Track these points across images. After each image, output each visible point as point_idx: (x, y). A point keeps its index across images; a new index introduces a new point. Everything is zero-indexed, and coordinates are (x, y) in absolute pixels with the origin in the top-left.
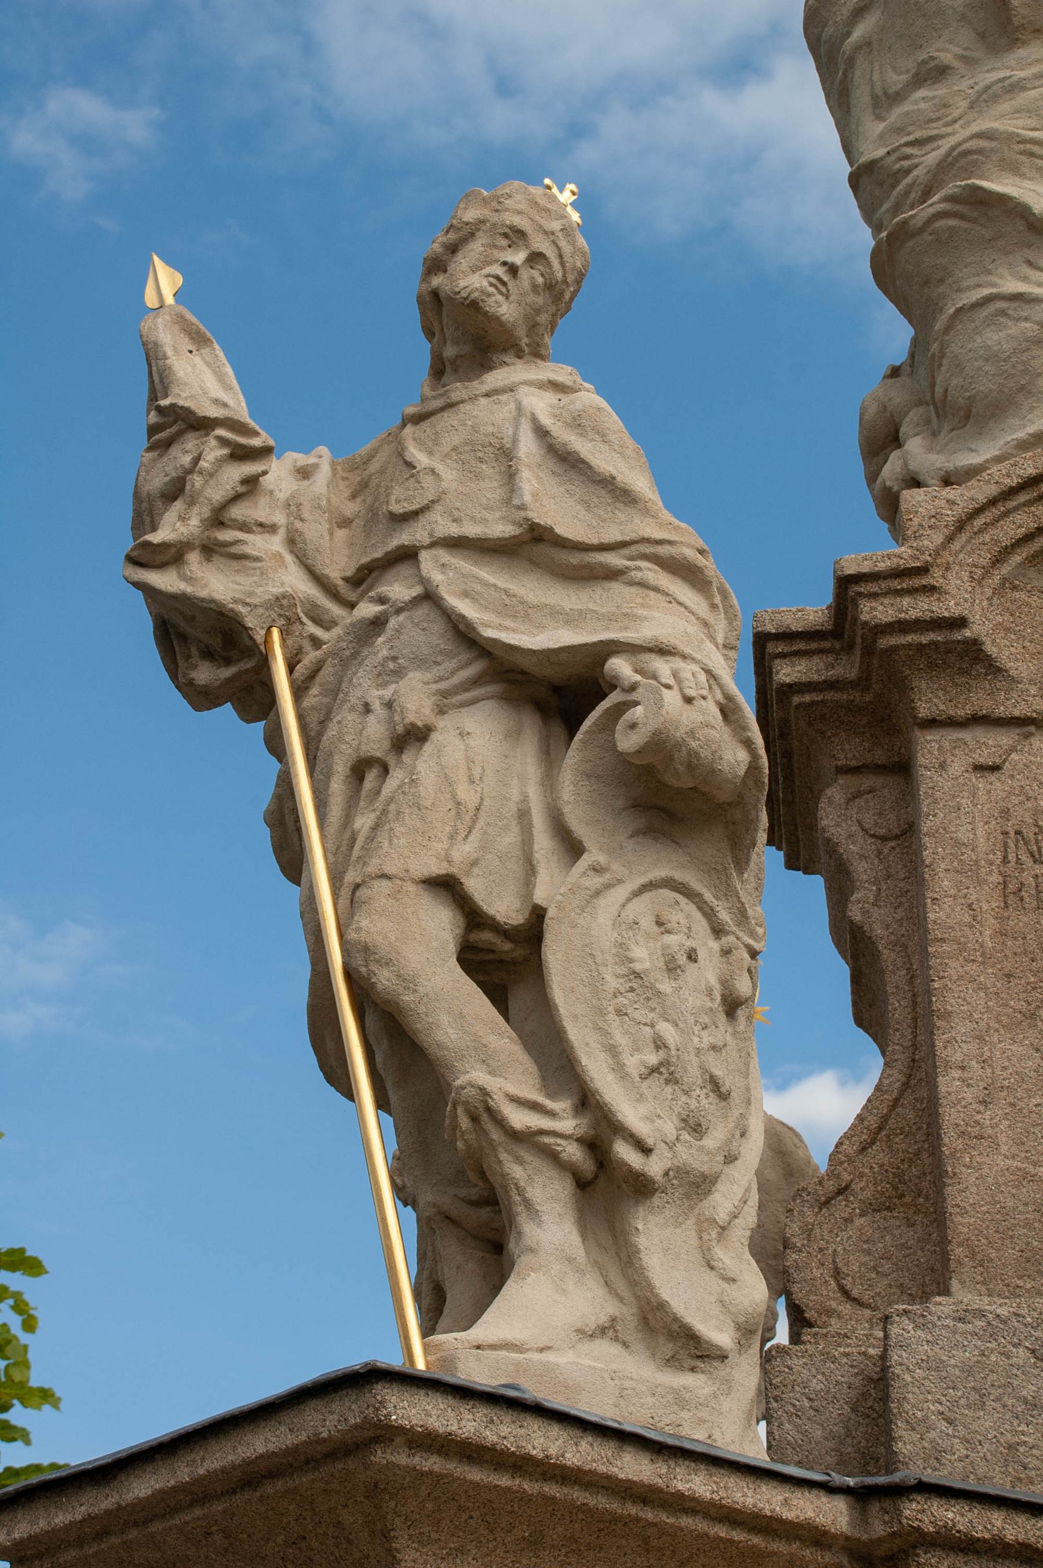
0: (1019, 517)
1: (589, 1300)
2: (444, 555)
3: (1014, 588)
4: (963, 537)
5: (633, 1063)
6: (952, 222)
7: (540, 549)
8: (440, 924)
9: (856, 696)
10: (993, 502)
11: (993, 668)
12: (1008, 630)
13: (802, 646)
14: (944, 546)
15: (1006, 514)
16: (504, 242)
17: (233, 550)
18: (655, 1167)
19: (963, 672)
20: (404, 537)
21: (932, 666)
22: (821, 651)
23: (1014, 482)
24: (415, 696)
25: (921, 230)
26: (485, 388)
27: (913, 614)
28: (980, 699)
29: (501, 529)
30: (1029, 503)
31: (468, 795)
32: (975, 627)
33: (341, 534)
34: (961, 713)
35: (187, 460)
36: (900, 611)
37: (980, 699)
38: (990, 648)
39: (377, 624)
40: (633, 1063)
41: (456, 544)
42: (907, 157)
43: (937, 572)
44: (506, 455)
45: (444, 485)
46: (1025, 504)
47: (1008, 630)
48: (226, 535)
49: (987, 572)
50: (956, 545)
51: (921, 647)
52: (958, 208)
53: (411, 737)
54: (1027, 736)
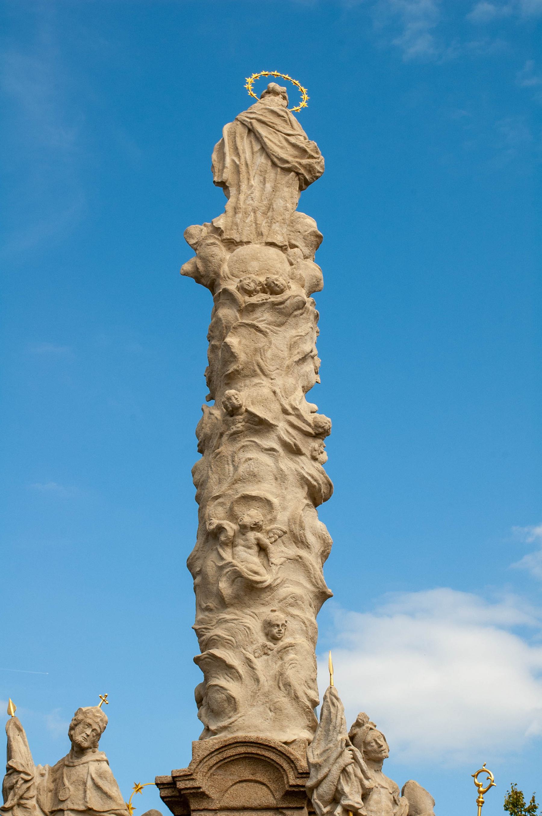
0: (214, 758)
2: (69, 812)
3: (214, 775)
4: (202, 764)
6: (209, 660)
7: (91, 812)
9: (179, 799)
10: (209, 755)
11: (208, 797)
12: (212, 786)
13: (166, 786)
14: (196, 768)
15: (212, 757)
16: (87, 727)
17: (24, 806)
19: (201, 798)
20: (61, 807)
21: (194, 797)
22: (170, 787)
23: (213, 750)
25: (203, 660)
26: (82, 762)
27: (189, 786)
28: (204, 805)
29: (82, 808)
30: (217, 754)
32: (203, 788)
33: (50, 794)
34: (201, 808)
35: (14, 781)
36: (186, 785)
37: (204, 805)
38: (207, 793)
42: (203, 632)
43: (194, 775)
44: (85, 784)
45: (71, 793)
46: (217, 754)
47: (212, 786)
48: (23, 802)
49: (207, 773)
50: (199, 767)
51: (191, 793)
52: (210, 657)
54: (216, 813)
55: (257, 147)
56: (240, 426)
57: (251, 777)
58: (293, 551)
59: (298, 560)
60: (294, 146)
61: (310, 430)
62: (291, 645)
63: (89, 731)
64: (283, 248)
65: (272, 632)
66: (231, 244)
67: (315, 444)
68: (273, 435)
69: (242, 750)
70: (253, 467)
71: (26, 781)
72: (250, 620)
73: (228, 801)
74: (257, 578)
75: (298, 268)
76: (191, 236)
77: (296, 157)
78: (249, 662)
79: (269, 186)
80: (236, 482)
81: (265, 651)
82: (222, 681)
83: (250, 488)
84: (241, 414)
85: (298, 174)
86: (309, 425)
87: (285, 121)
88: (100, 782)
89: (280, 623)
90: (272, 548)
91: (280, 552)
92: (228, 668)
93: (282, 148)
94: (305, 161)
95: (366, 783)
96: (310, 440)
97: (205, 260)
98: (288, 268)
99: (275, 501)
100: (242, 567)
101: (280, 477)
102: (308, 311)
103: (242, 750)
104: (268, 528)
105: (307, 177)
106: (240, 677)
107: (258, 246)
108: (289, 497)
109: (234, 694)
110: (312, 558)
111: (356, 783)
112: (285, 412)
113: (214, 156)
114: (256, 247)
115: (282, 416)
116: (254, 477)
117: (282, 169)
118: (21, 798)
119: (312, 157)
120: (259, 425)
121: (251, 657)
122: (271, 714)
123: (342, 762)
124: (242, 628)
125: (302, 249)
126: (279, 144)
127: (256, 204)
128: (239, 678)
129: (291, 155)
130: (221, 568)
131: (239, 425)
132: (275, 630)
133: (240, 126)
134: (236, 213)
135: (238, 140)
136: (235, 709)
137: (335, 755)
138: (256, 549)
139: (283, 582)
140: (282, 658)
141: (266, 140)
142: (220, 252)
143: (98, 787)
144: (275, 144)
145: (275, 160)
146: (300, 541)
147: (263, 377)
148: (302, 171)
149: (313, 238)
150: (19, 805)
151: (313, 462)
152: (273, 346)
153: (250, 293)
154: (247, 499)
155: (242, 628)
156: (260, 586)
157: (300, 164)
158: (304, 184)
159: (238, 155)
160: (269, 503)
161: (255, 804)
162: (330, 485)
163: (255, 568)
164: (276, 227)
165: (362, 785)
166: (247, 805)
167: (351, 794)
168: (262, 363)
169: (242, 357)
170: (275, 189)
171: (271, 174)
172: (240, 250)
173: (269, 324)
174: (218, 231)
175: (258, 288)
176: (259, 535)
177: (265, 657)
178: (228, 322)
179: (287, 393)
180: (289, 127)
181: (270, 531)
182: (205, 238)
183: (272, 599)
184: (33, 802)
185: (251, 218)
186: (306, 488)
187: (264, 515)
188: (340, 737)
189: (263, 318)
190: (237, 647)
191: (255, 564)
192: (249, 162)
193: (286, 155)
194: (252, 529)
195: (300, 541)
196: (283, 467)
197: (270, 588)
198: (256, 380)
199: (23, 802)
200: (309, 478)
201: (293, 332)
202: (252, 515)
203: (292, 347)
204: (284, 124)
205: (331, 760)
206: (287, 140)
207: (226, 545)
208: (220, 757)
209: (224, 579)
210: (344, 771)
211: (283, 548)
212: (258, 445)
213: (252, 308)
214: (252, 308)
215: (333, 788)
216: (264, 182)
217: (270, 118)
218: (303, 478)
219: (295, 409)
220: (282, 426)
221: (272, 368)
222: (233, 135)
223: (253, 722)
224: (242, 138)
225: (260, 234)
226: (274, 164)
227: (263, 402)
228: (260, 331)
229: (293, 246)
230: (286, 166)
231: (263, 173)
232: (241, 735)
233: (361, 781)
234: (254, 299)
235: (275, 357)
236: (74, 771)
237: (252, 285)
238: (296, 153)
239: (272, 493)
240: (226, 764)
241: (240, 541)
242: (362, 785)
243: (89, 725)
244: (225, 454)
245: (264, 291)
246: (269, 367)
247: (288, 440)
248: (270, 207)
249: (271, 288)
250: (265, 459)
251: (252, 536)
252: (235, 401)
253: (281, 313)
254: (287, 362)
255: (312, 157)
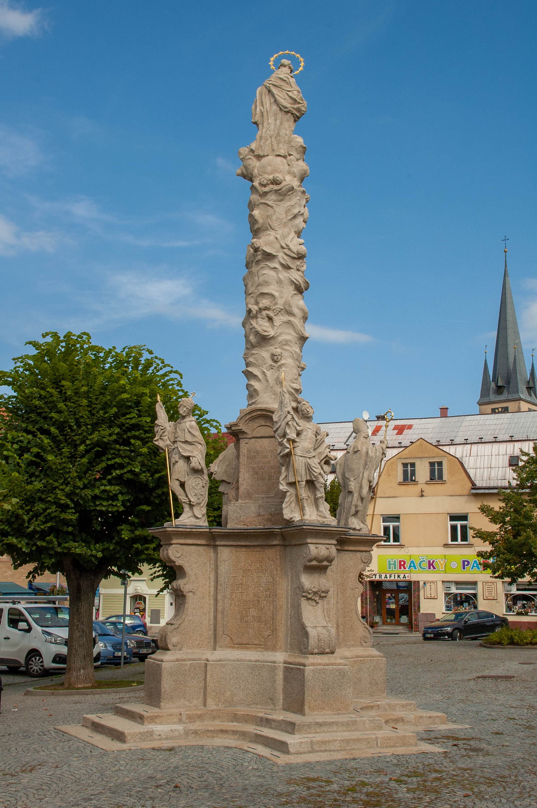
1: (190, 514)
5: (193, 495)
8: (177, 483)
11: (246, 433)
18: (194, 504)
24: (177, 459)
28: (245, 436)
29: (184, 440)
31: (180, 470)
37: (245, 436)
39: (174, 449)
40: (193, 495)
41: (180, 441)
48: (162, 437)
53: (177, 462)
55: (272, 100)
56: (259, 257)
57: (264, 424)
58: (286, 318)
59: (289, 323)
60: (291, 97)
61: (295, 256)
62: (283, 364)
63: (185, 409)
64: (285, 157)
65: (275, 358)
66: (259, 157)
67: (298, 263)
68: (277, 261)
69: (259, 413)
70: (265, 278)
71: (162, 430)
72: (265, 353)
73: (255, 434)
74: (266, 334)
75: (292, 167)
76: (240, 154)
77: (291, 104)
78: (264, 373)
79: (278, 122)
80: (258, 285)
81: (272, 367)
82: (252, 383)
83: (265, 289)
84: (260, 251)
85: (292, 114)
86: (295, 253)
87: (287, 83)
88: (191, 430)
89: (277, 354)
90: (275, 318)
91: (278, 320)
92: (255, 377)
93: (285, 99)
94: (296, 106)
95: (298, 428)
96: (296, 261)
97: (246, 167)
98: (287, 167)
99: (276, 294)
100: (259, 329)
101: (280, 282)
102: (296, 191)
103: (259, 413)
104: (273, 308)
105: (298, 115)
106: (260, 380)
107: (272, 157)
108: (284, 291)
109: (257, 388)
110: (297, 321)
111: (293, 428)
112: (282, 247)
113: (253, 107)
114: (271, 157)
115: (281, 250)
116: (266, 283)
117: (285, 111)
118: (161, 436)
119: (299, 103)
120: (269, 257)
121: (265, 370)
122: (273, 396)
123: (286, 420)
124: (261, 357)
125: (296, 155)
126: (283, 97)
127: (272, 133)
128: (259, 380)
129: (289, 103)
130: (251, 329)
131: (259, 257)
132: (276, 358)
133: (265, 89)
134: (261, 140)
135: (263, 97)
136: (258, 395)
137: (283, 417)
138: (267, 319)
139: (280, 334)
140: (279, 371)
141: (276, 96)
142: (254, 163)
143: (190, 432)
144: (281, 98)
145: (281, 107)
146: (290, 313)
147: (271, 230)
148: (295, 112)
149: (301, 149)
150: (161, 439)
151: (298, 272)
152: (277, 213)
153: (265, 186)
154: (263, 294)
155: (261, 357)
156: (268, 337)
157: (293, 108)
158: (296, 119)
159: (263, 106)
160: (272, 296)
161: (267, 435)
162: (307, 283)
163: (265, 329)
164: (281, 145)
165: (296, 429)
166: (263, 436)
167: (290, 433)
168: (271, 223)
169: (261, 221)
170: (281, 123)
171: (280, 115)
172: (264, 160)
173: (274, 201)
174: (252, 151)
175: (269, 182)
176: (267, 312)
177: (272, 370)
178: (255, 202)
179: (284, 237)
180: (289, 86)
181: (275, 309)
182: (246, 155)
183: (275, 343)
184: (167, 437)
185: (269, 141)
186: (294, 286)
187: (271, 302)
188: (286, 410)
189: (271, 199)
190: (259, 366)
191: (266, 327)
192: (268, 110)
193: (287, 104)
194: (264, 310)
195: (290, 313)
196: (280, 277)
197: (273, 337)
198: (268, 232)
199: (162, 437)
200: (295, 281)
201: (288, 204)
202: (265, 302)
203: (286, 212)
204: (287, 85)
205: (282, 420)
206: (287, 94)
207: (253, 318)
208: (250, 416)
209: (252, 335)
210: (287, 424)
211: (282, 317)
212: (269, 266)
213: (265, 194)
214: (265, 194)
215: (283, 431)
216: (276, 120)
217: (279, 83)
218: (292, 281)
219: (287, 245)
220: (281, 255)
221: (276, 225)
222: (261, 94)
223: (267, 401)
224: (265, 95)
225: (273, 150)
226: (281, 109)
227: (269, 244)
228: (269, 206)
229: (290, 155)
230: (286, 110)
231: (275, 115)
232: (259, 406)
233: (295, 427)
234: (266, 189)
235: (278, 218)
236: (181, 425)
237: (265, 181)
238: (292, 102)
239: (275, 290)
240: (253, 419)
241: (259, 316)
242: (296, 429)
243: (185, 406)
244: (254, 271)
245: (273, 184)
246: (275, 224)
247: (283, 262)
248: (278, 135)
249: (275, 182)
250: (272, 273)
251: (264, 313)
252: (256, 245)
253: (280, 195)
254: (285, 221)
255: (299, 103)
